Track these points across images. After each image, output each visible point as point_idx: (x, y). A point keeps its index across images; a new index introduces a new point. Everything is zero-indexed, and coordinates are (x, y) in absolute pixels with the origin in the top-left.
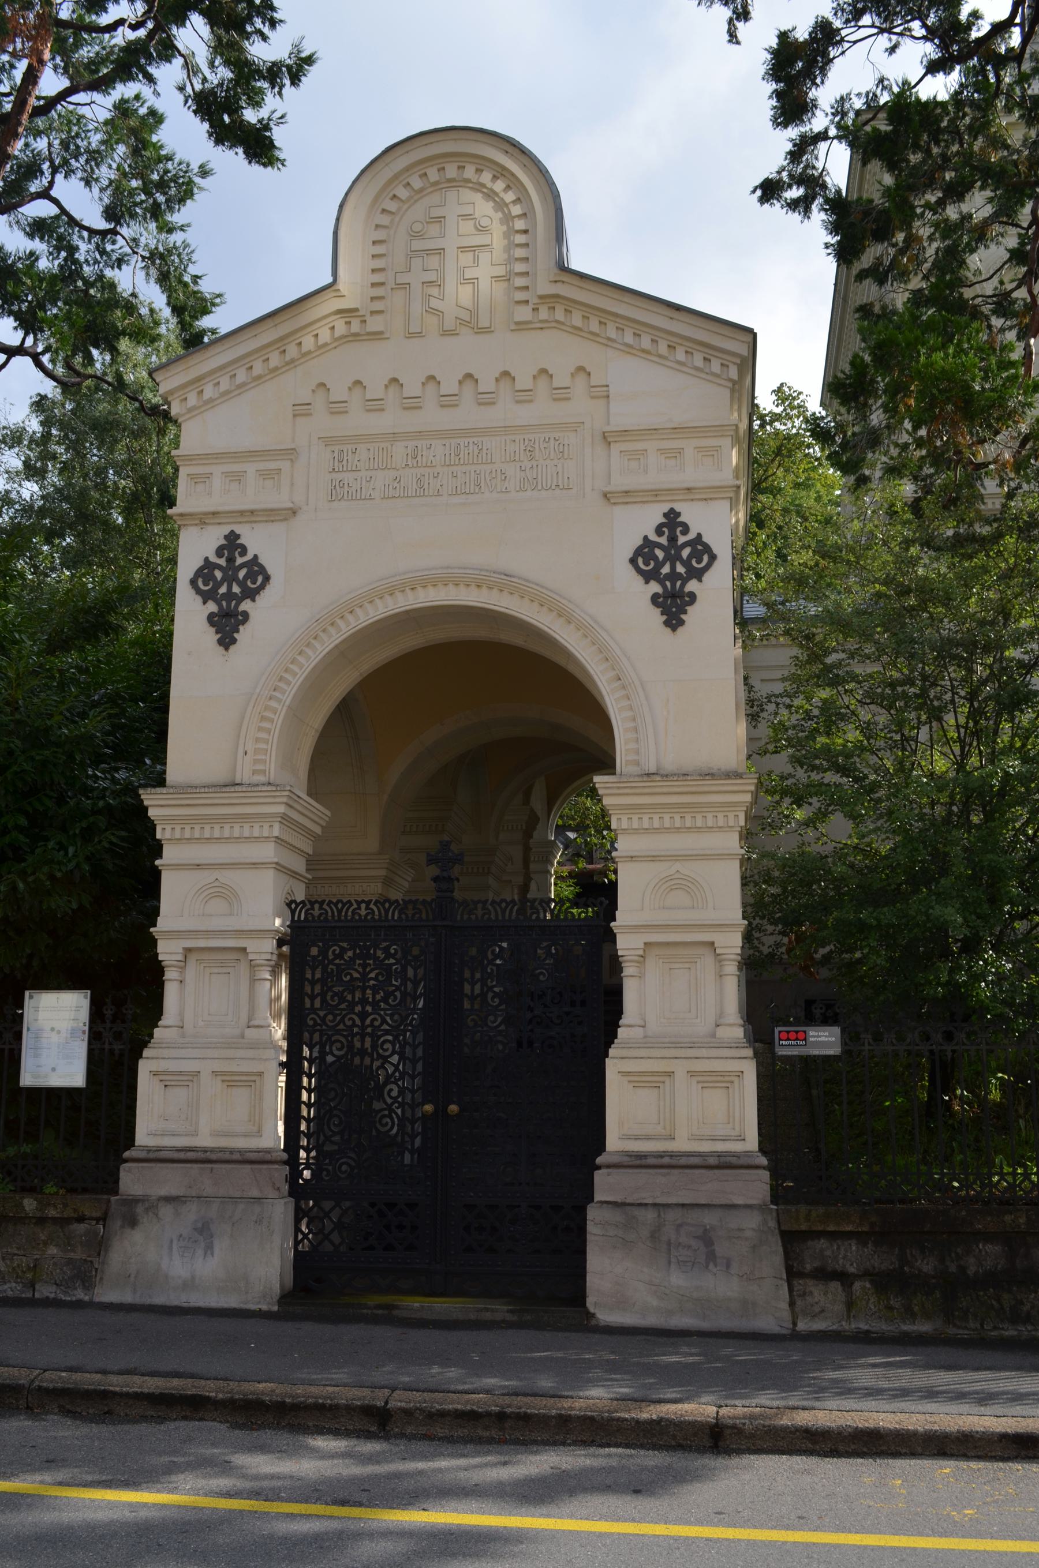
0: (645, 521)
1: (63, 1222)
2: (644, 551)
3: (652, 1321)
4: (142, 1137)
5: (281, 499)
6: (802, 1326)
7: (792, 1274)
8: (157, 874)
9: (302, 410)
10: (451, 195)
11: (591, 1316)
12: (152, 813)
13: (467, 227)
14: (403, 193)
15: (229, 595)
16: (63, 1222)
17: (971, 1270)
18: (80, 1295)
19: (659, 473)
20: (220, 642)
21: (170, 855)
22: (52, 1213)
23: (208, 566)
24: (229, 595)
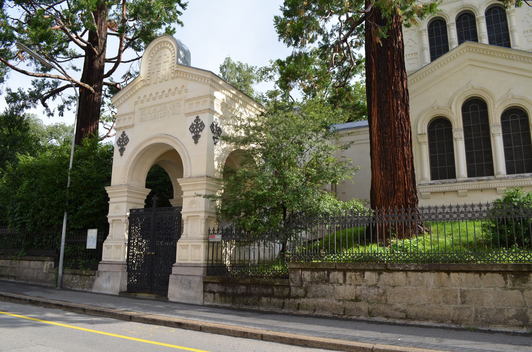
0: (191, 120)
1: (89, 276)
2: (192, 126)
3: (178, 301)
4: (103, 259)
5: (130, 123)
6: (205, 303)
7: (204, 291)
8: (109, 204)
9: (136, 103)
10: (163, 50)
11: (168, 299)
12: (180, 184)
13: (165, 57)
14: (154, 52)
15: (197, 131)
16: (89, 276)
17: (239, 292)
18: (90, 290)
19: (194, 109)
20: (195, 143)
21: (111, 200)
22: (87, 274)
23: (193, 124)
24: (197, 131)
